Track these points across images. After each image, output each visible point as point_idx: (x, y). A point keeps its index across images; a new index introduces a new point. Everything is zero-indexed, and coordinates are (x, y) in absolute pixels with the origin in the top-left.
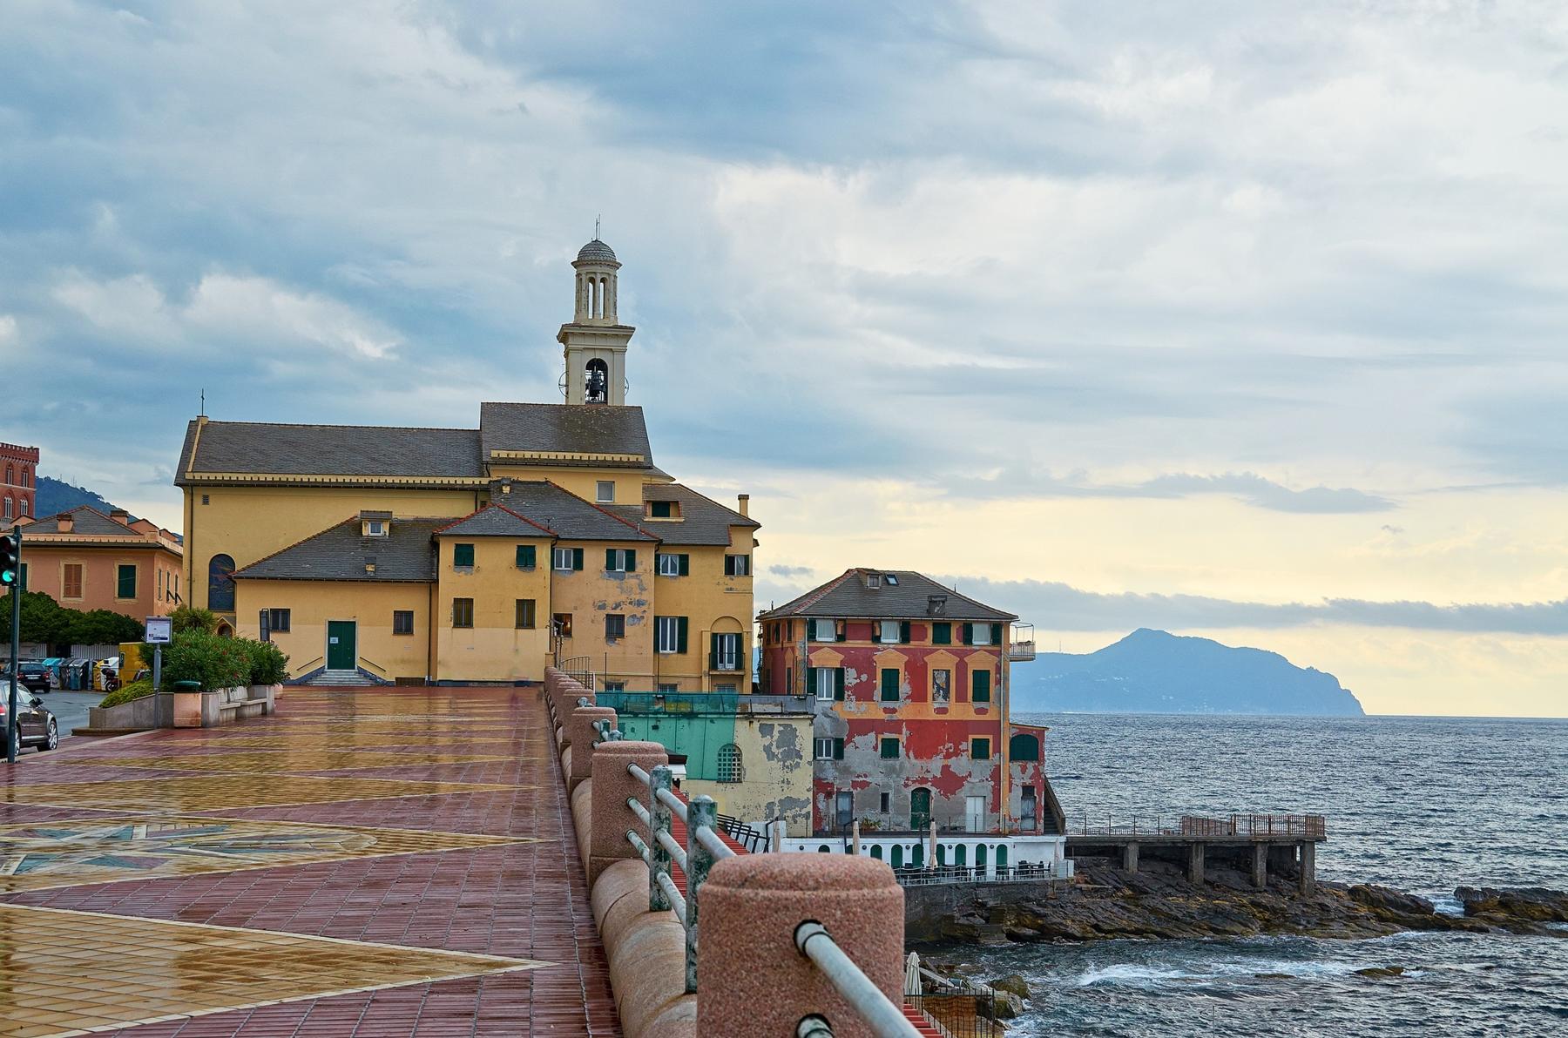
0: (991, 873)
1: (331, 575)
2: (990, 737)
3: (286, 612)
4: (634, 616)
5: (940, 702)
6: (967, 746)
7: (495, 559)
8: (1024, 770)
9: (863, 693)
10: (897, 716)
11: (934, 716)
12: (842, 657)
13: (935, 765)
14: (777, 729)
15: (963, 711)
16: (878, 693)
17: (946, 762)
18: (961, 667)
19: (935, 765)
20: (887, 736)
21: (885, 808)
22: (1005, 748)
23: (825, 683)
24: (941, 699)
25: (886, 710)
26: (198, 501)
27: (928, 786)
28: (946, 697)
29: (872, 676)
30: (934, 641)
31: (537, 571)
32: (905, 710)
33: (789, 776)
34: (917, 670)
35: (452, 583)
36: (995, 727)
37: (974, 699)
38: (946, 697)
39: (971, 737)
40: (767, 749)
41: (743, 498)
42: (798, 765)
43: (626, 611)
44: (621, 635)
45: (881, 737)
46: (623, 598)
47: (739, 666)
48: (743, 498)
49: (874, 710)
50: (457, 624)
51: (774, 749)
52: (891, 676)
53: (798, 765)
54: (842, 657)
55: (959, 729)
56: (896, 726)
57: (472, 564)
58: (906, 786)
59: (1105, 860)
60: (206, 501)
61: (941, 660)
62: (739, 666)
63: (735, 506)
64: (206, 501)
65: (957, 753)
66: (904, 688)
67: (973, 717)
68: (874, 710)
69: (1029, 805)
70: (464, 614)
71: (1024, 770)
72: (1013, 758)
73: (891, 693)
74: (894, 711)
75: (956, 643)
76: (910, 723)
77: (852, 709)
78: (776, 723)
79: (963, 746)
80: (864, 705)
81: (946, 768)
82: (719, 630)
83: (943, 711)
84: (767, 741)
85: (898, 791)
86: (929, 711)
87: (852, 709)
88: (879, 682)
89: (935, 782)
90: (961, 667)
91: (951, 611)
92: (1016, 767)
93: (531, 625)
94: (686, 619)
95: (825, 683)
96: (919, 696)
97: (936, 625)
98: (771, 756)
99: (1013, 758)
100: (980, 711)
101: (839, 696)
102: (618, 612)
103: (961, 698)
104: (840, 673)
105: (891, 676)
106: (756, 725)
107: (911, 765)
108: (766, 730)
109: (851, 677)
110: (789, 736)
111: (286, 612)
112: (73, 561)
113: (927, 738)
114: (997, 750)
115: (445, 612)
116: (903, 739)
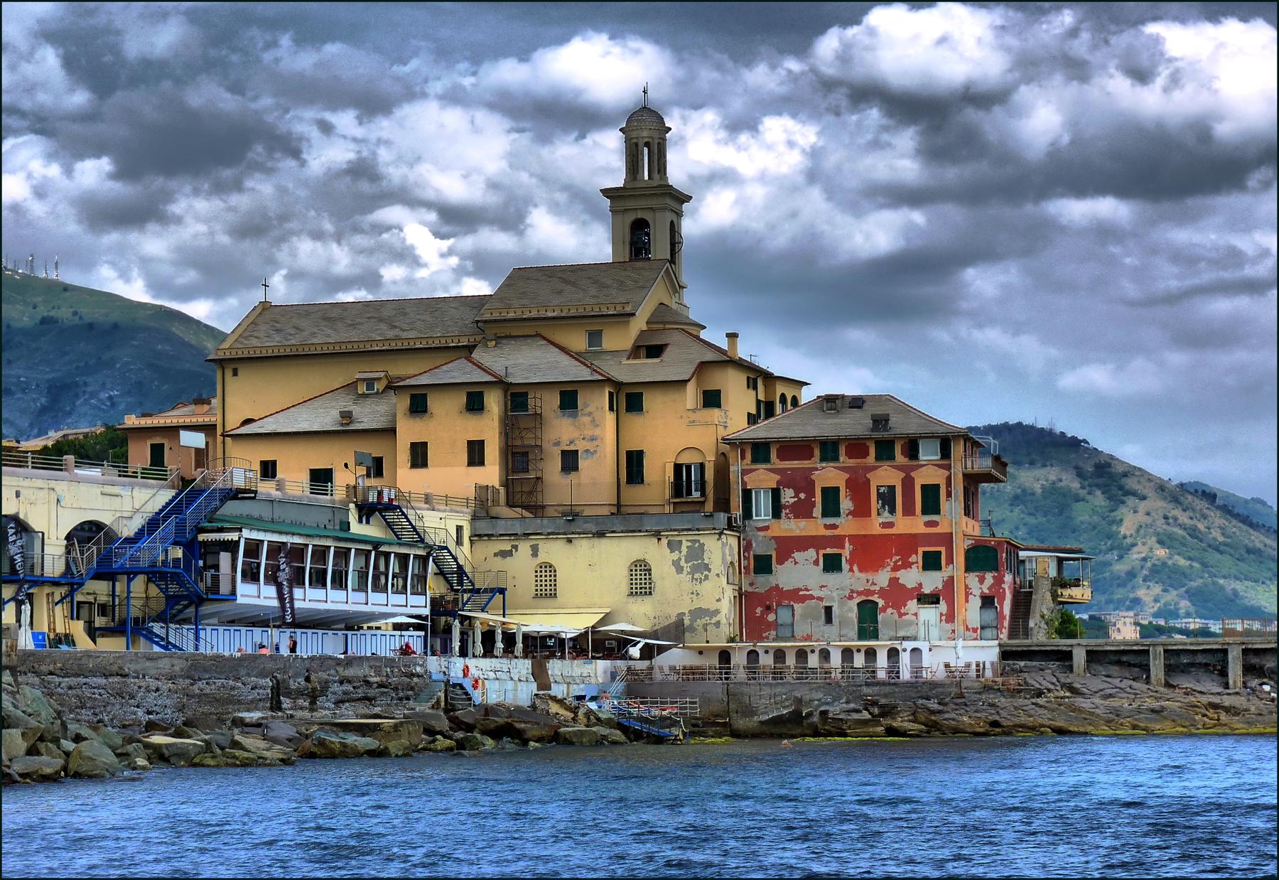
0: (906, 675)
1: (315, 428)
2: (943, 549)
3: (274, 463)
4: (587, 451)
5: (886, 517)
6: (918, 558)
7: (597, 404)
8: (982, 581)
9: (802, 510)
10: (836, 532)
11: (878, 530)
12: (778, 477)
13: (882, 578)
14: (685, 544)
15: (915, 524)
16: (817, 511)
17: (894, 575)
18: (908, 483)
19: (882, 578)
20: (829, 551)
21: (829, 620)
22: (959, 559)
23: (763, 504)
24: (886, 514)
25: (827, 527)
26: (229, 373)
27: (875, 598)
28: (892, 511)
29: (811, 493)
30: (878, 458)
31: (485, 415)
32: (846, 525)
33: (698, 587)
34: (859, 487)
35: (409, 430)
36: (947, 539)
37: (924, 512)
38: (892, 511)
39: (921, 550)
40: (677, 565)
41: (732, 336)
42: (707, 577)
43: (580, 446)
44: (576, 468)
45: (822, 552)
46: (576, 434)
47: (703, 494)
48: (732, 336)
49: (915, 524)
50: (414, 465)
51: (683, 563)
52: (831, 496)
53: (707, 577)
54: (778, 477)
55: (907, 544)
56: (838, 541)
57: (425, 411)
58: (851, 598)
59: (1054, 665)
60: (235, 373)
61: (885, 476)
62: (703, 494)
63: (723, 344)
64: (235, 373)
65: (907, 565)
66: (846, 504)
67: (922, 529)
68: (815, 526)
69: (990, 615)
70: (419, 456)
71: (982, 581)
72: (968, 569)
73: (831, 508)
74: (834, 527)
75: (900, 458)
76: (854, 539)
77: (791, 527)
78: (684, 539)
79: (913, 558)
80: (803, 523)
81: (894, 582)
82: (685, 459)
83: (890, 525)
84: (675, 556)
85: (841, 605)
86: (875, 524)
87: (791, 527)
88: (818, 498)
89: (882, 593)
90: (908, 483)
91: (900, 427)
92: (973, 579)
93: (482, 463)
94: (640, 454)
95: (763, 504)
96: (861, 511)
97: (879, 443)
98: (679, 570)
99: (968, 569)
100: (928, 524)
101: (776, 514)
102: (572, 448)
103: (909, 511)
104: (776, 494)
105: (831, 496)
106: (664, 541)
107: (851, 579)
108: (673, 546)
109: (788, 496)
110: (697, 553)
111: (274, 463)
112: (157, 441)
113: (871, 552)
114: (950, 560)
115: (403, 455)
116: (846, 552)
